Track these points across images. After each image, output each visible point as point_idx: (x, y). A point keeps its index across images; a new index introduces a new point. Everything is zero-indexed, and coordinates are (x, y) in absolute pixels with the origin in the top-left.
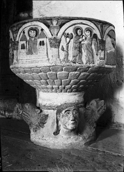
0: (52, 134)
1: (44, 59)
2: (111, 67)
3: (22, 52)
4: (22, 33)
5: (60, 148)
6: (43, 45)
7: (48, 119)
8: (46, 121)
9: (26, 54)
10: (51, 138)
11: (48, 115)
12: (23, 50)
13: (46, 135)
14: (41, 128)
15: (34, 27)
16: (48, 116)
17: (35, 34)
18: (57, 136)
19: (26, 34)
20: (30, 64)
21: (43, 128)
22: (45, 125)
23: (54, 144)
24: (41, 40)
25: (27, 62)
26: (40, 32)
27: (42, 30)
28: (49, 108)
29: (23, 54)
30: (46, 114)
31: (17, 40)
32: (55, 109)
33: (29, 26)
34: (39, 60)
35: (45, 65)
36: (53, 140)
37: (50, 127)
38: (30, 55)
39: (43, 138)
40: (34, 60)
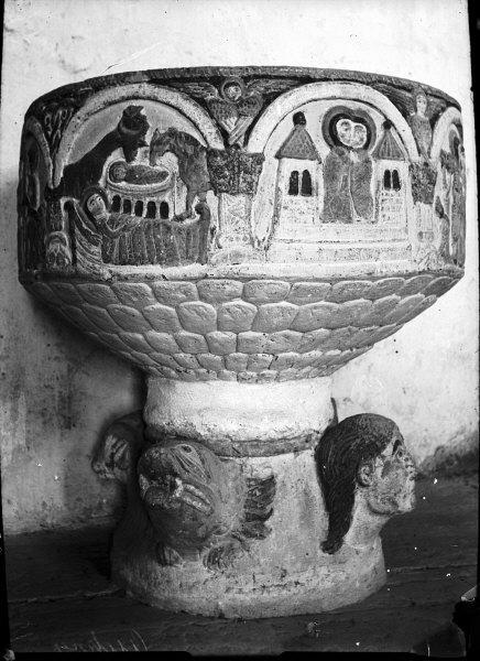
0: (320, 553)
1: (396, 244)
2: (38, 186)
3: (291, 206)
4: (289, 124)
5: (367, 592)
6: (397, 186)
7: (279, 494)
8: (268, 508)
9: (317, 220)
10: (323, 571)
11: (271, 480)
12: (299, 198)
13: (293, 564)
14: (255, 544)
15: (353, 106)
16: (275, 484)
17: (365, 139)
18: (340, 555)
19: (314, 127)
20: (339, 265)
21: (262, 537)
22: (267, 523)
23: (336, 589)
24: (390, 165)
25: (324, 254)
26: (380, 133)
27: (388, 125)
28: (280, 445)
29: (303, 217)
30: (264, 474)
31: (254, 146)
32: (304, 449)
33: (334, 98)
34: (379, 245)
35: (403, 270)
36: (333, 575)
37: (294, 527)
38: (339, 225)
39: (286, 580)
40: (359, 246)
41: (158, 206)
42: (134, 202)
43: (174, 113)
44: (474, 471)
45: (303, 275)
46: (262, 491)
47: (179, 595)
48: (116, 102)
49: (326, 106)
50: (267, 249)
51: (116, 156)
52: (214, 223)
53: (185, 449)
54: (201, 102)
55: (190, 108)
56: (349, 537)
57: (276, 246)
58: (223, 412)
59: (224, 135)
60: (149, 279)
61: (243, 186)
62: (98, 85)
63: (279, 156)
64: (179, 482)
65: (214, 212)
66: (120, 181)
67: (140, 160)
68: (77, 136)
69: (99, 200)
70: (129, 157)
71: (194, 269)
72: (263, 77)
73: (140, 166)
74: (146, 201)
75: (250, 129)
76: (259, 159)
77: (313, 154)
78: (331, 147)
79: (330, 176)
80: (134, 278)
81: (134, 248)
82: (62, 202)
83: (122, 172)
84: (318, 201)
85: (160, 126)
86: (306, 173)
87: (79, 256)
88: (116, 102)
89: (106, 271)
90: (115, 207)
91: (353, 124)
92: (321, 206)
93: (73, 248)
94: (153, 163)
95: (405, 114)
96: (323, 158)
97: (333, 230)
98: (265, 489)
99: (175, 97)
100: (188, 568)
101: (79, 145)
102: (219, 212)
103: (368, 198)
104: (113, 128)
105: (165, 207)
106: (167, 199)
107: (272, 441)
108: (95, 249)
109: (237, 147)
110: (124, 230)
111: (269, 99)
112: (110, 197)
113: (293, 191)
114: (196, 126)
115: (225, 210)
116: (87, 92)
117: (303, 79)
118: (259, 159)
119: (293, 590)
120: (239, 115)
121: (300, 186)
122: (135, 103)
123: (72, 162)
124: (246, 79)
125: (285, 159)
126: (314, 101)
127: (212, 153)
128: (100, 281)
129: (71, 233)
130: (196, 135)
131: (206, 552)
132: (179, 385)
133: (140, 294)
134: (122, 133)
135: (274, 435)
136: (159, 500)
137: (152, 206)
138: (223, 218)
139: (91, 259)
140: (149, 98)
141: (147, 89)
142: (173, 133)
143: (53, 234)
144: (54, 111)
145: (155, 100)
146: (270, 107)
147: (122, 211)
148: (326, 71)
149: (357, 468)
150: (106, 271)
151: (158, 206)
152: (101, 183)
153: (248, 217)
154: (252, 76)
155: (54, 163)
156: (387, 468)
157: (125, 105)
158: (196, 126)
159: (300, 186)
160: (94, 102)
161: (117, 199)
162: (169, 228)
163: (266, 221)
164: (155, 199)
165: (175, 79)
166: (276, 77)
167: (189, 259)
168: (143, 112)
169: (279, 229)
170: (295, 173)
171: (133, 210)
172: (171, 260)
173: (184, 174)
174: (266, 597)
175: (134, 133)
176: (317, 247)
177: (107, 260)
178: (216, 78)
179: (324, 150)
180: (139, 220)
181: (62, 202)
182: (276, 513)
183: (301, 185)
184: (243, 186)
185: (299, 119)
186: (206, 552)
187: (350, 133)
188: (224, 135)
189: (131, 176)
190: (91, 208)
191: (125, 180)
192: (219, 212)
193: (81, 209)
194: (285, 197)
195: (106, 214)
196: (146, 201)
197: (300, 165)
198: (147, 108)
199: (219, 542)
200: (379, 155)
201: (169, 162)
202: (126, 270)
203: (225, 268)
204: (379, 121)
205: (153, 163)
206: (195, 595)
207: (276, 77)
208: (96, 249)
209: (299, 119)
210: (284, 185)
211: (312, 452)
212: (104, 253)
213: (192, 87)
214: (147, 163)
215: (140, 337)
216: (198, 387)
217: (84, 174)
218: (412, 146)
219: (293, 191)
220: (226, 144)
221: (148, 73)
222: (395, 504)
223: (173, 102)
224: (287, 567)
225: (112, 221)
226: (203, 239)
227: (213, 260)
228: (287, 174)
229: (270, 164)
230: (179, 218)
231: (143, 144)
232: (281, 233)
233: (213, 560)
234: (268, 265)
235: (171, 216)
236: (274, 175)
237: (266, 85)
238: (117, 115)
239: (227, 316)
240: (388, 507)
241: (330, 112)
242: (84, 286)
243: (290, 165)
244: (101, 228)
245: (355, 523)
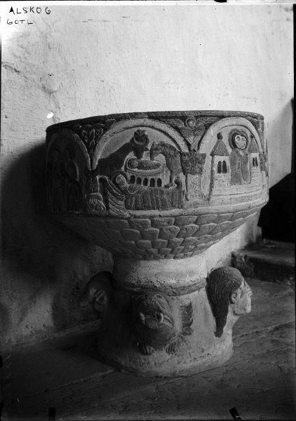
7: (194, 312)
12: (222, 174)
14: (187, 338)
19: (225, 140)
22: (191, 327)
26: (249, 140)
27: (252, 136)
30: (187, 303)
31: (202, 151)
39: (204, 354)
41: (156, 181)
42: (143, 179)
43: (162, 135)
44: (290, 294)
45: (224, 211)
46: (188, 311)
47: (155, 369)
48: (131, 128)
49: (230, 129)
50: (209, 199)
51: (131, 155)
52: (184, 188)
53: (159, 297)
54: (177, 129)
55: (171, 132)
57: (213, 198)
58: (168, 275)
59: (188, 145)
60: (151, 217)
61: (198, 170)
62: (119, 118)
63: (212, 155)
64: (162, 315)
65: (184, 183)
66: (135, 168)
67: (145, 157)
68: (106, 143)
69: (123, 178)
70: (139, 155)
71: (176, 211)
72: (204, 116)
73: (146, 161)
74: (150, 179)
75: (200, 141)
76: (204, 156)
78: (232, 149)
79: (233, 163)
80: (144, 217)
81: (144, 202)
82: (98, 178)
83: (136, 163)
84: (228, 175)
85: (155, 140)
86: (224, 162)
87: (110, 206)
88: (131, 128)
89: (127, 214)
90: (132, 180)
91: (241, 137)
92: (230, 177)
93: (106, 202)
94: (152, 159)
96: (230, 154)
97: (234, 189)
98: (188, 309)
100: (158, 355)
101: (107, 149)
102: (186, 184)
103: (247, 172)
104: (128, 141)
105: (160, 181)
106: (161, 178)
107: (190, 286)
108: (120, 202)
109: (194, 150)
110: (138, 193)
111: (207, 127)
112: (129, 177)
113: (219, 171)
114: (174, 141)
115: (190, 182)
116: (112, 122)
117: (221, 116)
118: (204, 156)
119: (207, 358)
120: (195, 135)
122: (141, 129)
123: (103, 157)
124: (197, 117)
125: (215, 156)
126: (224, 127)
127: (182, 154)
128: (123, 218)
129: (105, 194)
130: (174, 145)
131: (168, 346)
132: (142, 262)
133: (145, 225)
134: (135, 144)
135: (191, 283)
137: (153, 180)
138: (189, 185)
139: (118, 208)
140: (149, 127)
141: (149, 122)
142: (163, 145)
143: (92, 194)
144: (90, 129)
145: (153, 127)
146: (208, 131)
147: (135, 183)
148: (229, 112)
149: (230, 295)
150: (127, 214)
151: (156, 181)
152: (123, 168)
153: (200, 186)
154: (200, 115)
155: (90, 157)
157: (136, 129)
158: (174, 141)
160: (117, 127)
161: (133, 177)
162: (163, 192)
163: (207, 187)
164: (154, 177)
165: (162, 117)
166: (210, 116)
167: (174, 207)
168: (146, 133)
169: (214, 190)
170: (220, 162)
171: (142, 183)
172: (164, 207)
173: (168, 165)
174: (196, 363)
175: (141, 144)
176: (229, 197)
177: (128, 207)
178: (183, 116)
179: (230, 150)
180: (146, 188)
181: (98, 178)
182: (194, 321)
183: (222, 168)
184: (198, 170)
185: (219, 136)
186: (168, 346)
187: (240, 141)
188: (188, 145)
189: (141, 166)
190: (118, 182)
191: (138, 168)
192: (186, 184)
193: (111, 182)
195: (127, 185)
196: (150, 179)
198: (148, 131)
199: (175, 339)
201: (160, 159)
202: (139, 213)
203: (191, 210)
205: (152, 159)
206: (163, 368)
207: (210, 116)
208: (122, 203)
209: (219, 136)
210: (215, 169)
211: (204, 289)
212: (126, 203)
213: (172, 121)
214: (148, 159)
215: (133, 242)
216: (153, 263)
219: (219, 171)
220: (190, 150)
221: (148, 113)
222: (245, 310)
223: (162, 129)
224: (203, 347)
225: (131, 189)
226: (180, 197)
227: (185, 207)
228: (216, 163)
230: (166, 187)
231: (147, 150)
232: (215, 192)
233: (171, 350)
234: (210, 207)
235: (163, 185)
237: (206, 119)
238: (129, 135)
239: (184, 231)
240: (242, 312)
241: (231, 133)
242: (111, 221)
243: (218, 159)
244: (124, 192)
245: (228, 321)
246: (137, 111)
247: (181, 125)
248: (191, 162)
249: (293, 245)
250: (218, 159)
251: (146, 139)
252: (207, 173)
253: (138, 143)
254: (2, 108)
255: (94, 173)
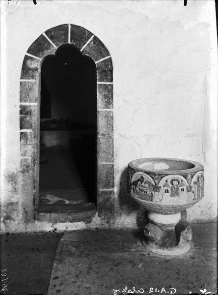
19: (169, 182)
24: (182, 187)
26: (180, 182)
38: (173, 197)
51: (140, 182)
54: (152, 177)
55: (150, 178)
56: (180, 243)
57: (163, 201)
63: (163, 186)
67: (143, 184)
70: (142, 183)
71: (151, 202)
76: (160, 187)
77: (168, 186)
79: (172, 190)
84: (169, 194)
95: (186, 178)
99: (148, 176)
105: (146, 192)
111: (162, 178)
113: (166, 192)
118: (160, 187)
121: (108, 83)
127: (153, 185)
136: (146, 235)
156: (186, 233)
159: (108, 83)
179: (171, 185)
183: (167, 191)
185: (167, 181)
187: (175, 183)
194: (164, 193)
197: (167, 188)
200: (180, 186)
201: (147, 185)
204: (180, 180)
209: (167, 181)
210: (164, 191)
217: (135, 183)
218: (187, 183)
219: (166, 192)
228: (165, 190)
229: (162, 188)
232: (164, 198)
236: (163, 190)
243: (165, 188)
246: (79, 25)
247: (153, 177)
248: (156, 188)
249: (215, 292)
250: (165, 188)
251: (143, 179)
252: (161, 192)
253: (141, 179)
254: (27, 1)
255: (131, 185)
